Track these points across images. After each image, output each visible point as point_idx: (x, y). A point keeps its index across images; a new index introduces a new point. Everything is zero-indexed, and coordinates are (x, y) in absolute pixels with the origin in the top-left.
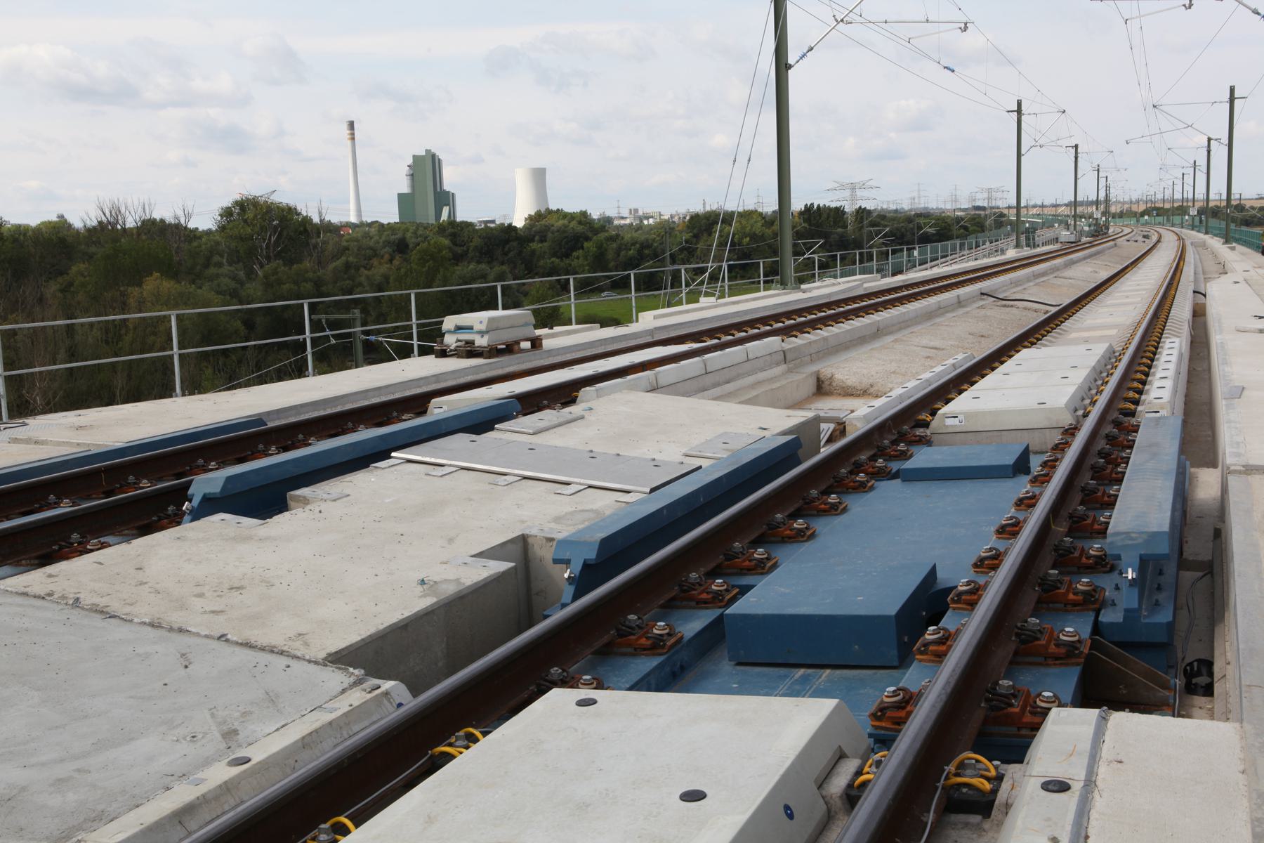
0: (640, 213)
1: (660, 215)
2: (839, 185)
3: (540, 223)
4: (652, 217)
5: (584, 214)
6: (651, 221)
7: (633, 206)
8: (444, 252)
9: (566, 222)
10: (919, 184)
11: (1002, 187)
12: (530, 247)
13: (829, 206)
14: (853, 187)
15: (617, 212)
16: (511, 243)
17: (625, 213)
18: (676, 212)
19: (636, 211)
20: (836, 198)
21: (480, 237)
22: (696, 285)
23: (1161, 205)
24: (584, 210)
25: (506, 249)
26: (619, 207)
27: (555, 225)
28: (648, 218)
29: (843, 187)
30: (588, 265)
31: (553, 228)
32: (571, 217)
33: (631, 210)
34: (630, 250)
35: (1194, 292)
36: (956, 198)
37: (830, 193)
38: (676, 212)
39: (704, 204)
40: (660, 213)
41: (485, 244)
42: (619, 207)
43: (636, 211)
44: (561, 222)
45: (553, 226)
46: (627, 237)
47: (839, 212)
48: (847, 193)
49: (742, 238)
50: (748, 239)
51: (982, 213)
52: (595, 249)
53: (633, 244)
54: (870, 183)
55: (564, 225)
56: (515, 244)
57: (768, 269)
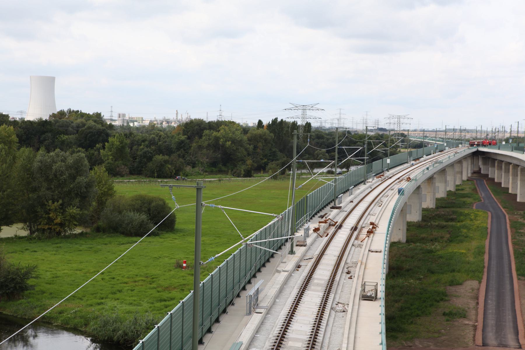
0: (127, 118)
1: (143, 120)
2: (294, 106)
3: (62, 119)
4: (136, 121)
5: (98, 115)
6: (136, 124)
7: (122, 112)
8: (13, 137)
9: (83, 120)
10: (367, 112)
11: (407, 115)
12: (61, 138)
13: (285, 121)
14: (304, 108)
15: (110, 115)
16: (46, 134)
17: (115, 117)
18: (155, 118)
19: (124, 115)
20: (291, 116)
21: (20, 127)
22: (350, 158)
23: (516, 135)
24: (99, 112)
25: (41, 139)
26: (112, 112)
27: (75, 122)
28: (133, 122)
29: (296, 108)
30: (111, 155)
31: (73, 124)
32: (87, 117)
33: (120, 115)
34: (141, 145)
35: (369, 251)
36: (366, 122)
37: (287, 111)
38: (155, 118)
39: (177, 114)
40: (142, 118)
41: (25, 133)
42: (112, 112)
43: (124, 115)
44: (79, 121)
45: (72, 122)
46: (139, 136)
47: (294, 124)
48: (299, 113)
49: (226, 141)
50: (230, 143)
51: (385, 133)
52: (118, 143)
53: (144, 141)
54: (317, 106)
55: (82, 122)
56: (50, 135)
57: (250, 166)
